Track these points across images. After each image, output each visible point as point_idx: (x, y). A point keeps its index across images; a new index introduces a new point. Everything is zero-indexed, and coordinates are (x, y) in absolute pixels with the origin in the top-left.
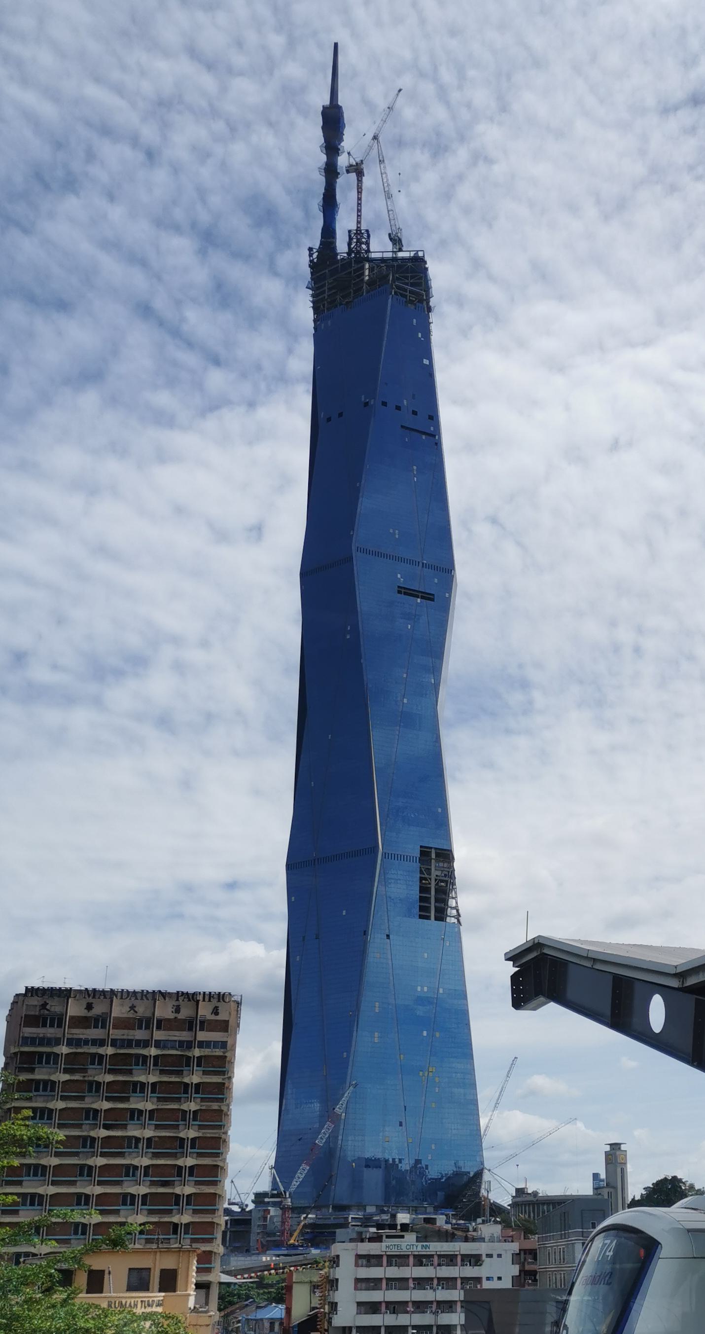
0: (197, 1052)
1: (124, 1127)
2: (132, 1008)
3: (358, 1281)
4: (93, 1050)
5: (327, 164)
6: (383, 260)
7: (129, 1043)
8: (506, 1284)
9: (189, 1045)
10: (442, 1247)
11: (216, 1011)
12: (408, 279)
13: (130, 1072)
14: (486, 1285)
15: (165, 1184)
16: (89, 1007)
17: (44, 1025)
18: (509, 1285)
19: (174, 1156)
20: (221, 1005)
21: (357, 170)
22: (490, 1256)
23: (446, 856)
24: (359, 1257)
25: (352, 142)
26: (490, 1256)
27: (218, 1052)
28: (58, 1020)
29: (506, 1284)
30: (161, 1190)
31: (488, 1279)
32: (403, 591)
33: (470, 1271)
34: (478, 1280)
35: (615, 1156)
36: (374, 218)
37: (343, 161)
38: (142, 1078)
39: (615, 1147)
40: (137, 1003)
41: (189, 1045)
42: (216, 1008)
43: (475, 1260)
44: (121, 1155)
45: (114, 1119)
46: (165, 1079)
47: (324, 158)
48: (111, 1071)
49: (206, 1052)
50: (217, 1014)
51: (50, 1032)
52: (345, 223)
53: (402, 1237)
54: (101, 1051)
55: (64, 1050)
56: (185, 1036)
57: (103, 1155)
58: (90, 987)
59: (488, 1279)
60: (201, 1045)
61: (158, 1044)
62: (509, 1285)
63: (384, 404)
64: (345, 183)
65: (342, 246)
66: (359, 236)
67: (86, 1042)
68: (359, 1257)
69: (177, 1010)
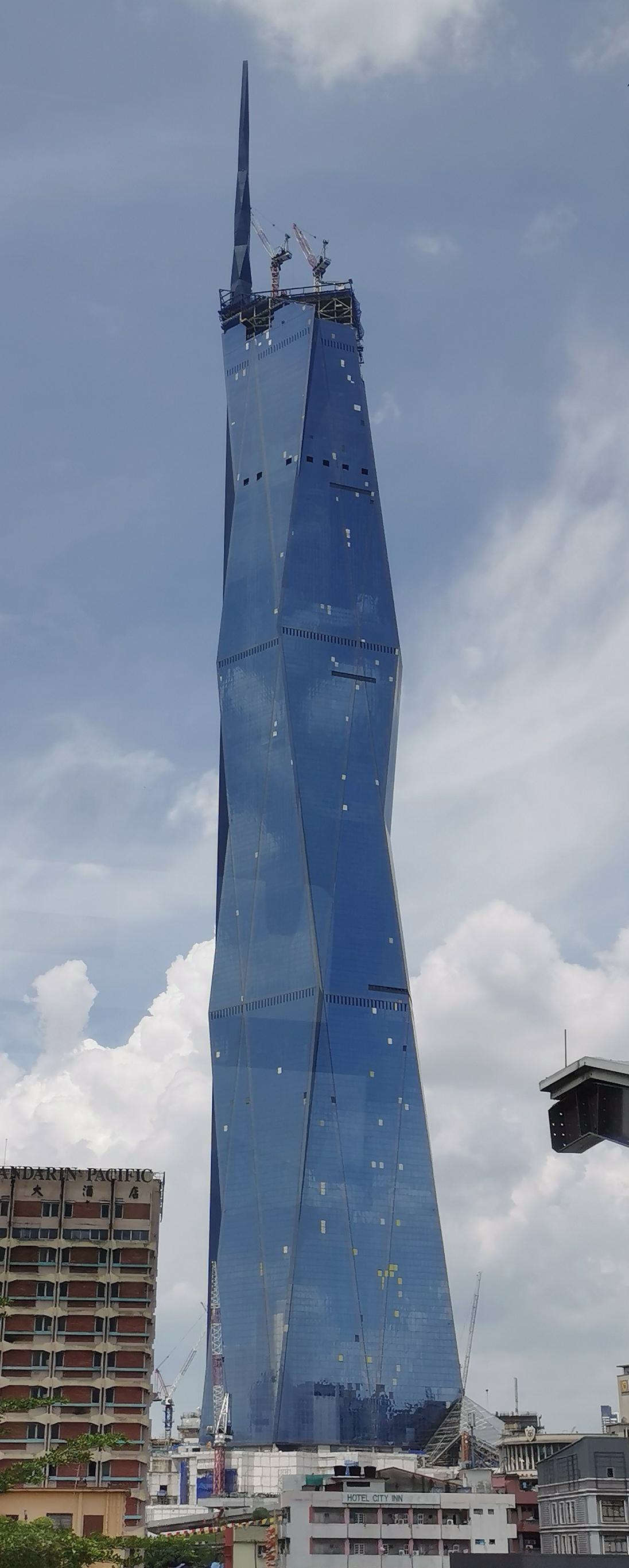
0: (113, 1244)
2: (37, 1189)
7: (34, 1234)
9: (104, 1235)
11: (134, 1193)
14: (476, 1549)
16: (89, 1192)
22: (479, 1511)
24: (315, 1510)
26: (479, 1511)
27: (139, 1244)
31: (478, 1541)
34: (466, 1543)
42: (135, 1189)
43: (461, 1516)
50: (136, 1196)
53: (368, 1485)
59: (478, 1541)
69: (89, 1192)
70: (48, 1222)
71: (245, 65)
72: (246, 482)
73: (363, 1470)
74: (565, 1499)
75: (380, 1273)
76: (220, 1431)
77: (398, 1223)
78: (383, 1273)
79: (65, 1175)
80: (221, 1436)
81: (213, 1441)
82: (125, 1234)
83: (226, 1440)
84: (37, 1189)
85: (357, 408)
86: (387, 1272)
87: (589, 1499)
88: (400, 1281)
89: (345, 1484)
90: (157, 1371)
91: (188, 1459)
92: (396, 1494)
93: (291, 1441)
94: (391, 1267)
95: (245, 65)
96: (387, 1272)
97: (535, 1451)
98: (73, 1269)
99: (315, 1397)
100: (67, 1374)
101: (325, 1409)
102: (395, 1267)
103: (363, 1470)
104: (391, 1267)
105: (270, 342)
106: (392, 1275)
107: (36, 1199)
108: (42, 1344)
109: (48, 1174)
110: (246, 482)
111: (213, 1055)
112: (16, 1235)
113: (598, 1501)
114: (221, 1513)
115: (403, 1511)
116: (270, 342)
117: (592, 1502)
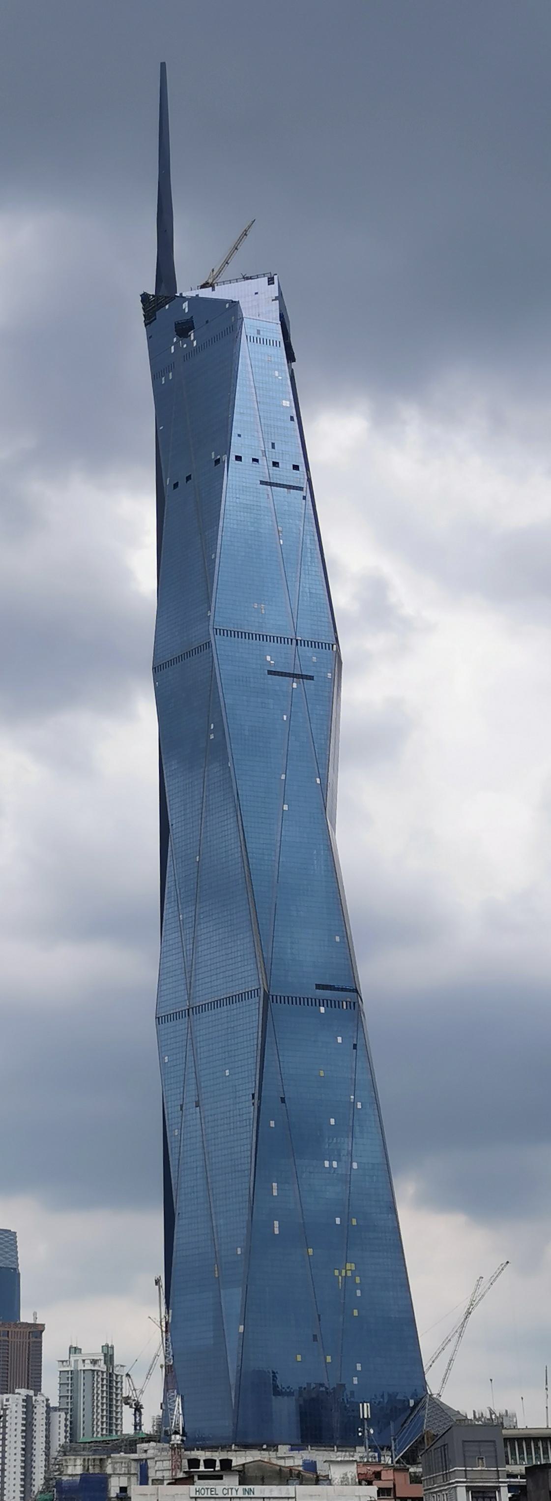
10: (271, 1491)
71: (163, 65)
72: (176, 485)
73: (218, 1463)
74: (441, 1491)
75: (337, 1272)
76: (176, 1433)
77: (354, 1222)
78: (340, 1273)
80: (178, 1437)
81: (169, 1441)
83: (182, 1440)
85: (227, 306)
86: (344, 1271)
87: (458, 1489)
88: (358, 1280)
89: (196, 1478)
90: (128, 1375)
91: (146, 1460)
92: (247, 1487)
93: (250, 1441)
94: (348, 1266)
95: (163, 65)
96: (344, 1271)
97: (537, 1448)
99: (273, 1397)
101: (285, 1410)
102: (353, 1267)
103: (218, 1463)
104: (348, 1266)
105: (195, 343)
106: (349, 1274)
110: (176, 485)
111: (161, 1058)
113: (467, 1491)
116: (195, 343)
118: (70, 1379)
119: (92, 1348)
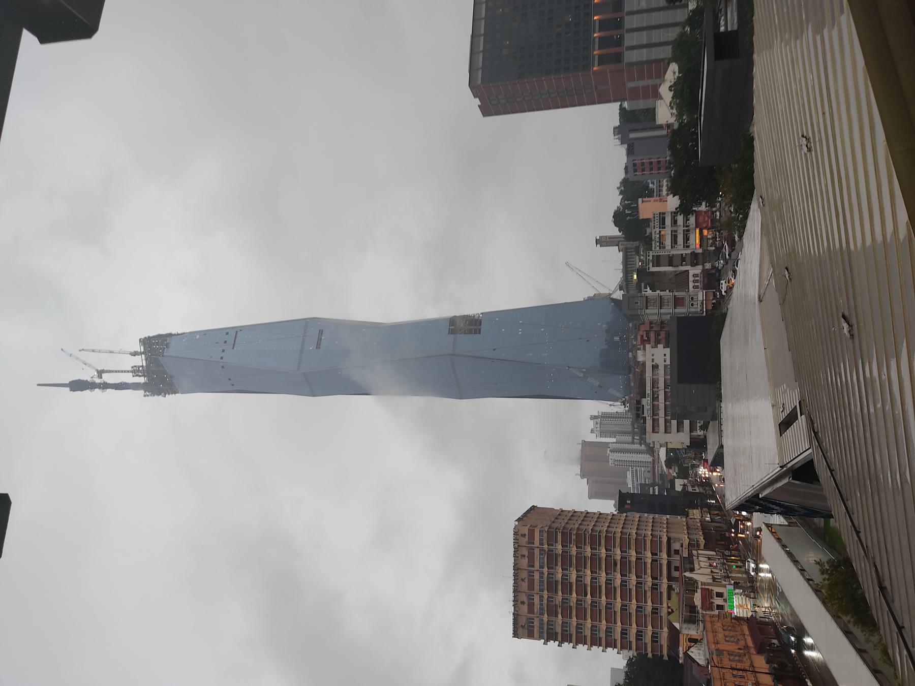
1: (585, 585)
2: (523, 580)
3: (666, 432)
4: (545, 602)
5: (100, 388)
6: (146, 359)
7: (541, 582)
8: (668, 351)
11: (524, 535)
12: (155, 346)
13: (556, 582)
14: (668, 362)
15: (615, 564)
16: (523, 603)
17: (533, 627)
18: (669, 349)
19: (600, 559)
20: (520, 533)
21: (100, 373)
22: (653, 360)
23: (453, 321)
24: (653, 431)
25: (87, 375)
26: (653, 360)
28: (530, 621)
29: (668, 351)
30: (619, 566)
32: (318, 346)
33: (661, 371)
34: (665, 366)
35: (602, 242)
36: (127, 362)
37: (98, 381)
38: (560, 576)
39: (597, 242)
40: (526, 539)
41: (542, 550)
43: (655, 367)
44: (600, 587)
45: (581, 590)
46: (560, 564)
47: (97, 390)
48: (556, 592)
49: (545, 541)
51: (536, 623)
52: (129, 378)
54: (546, 597)
55: (545, 618)
56: (537, 552)
57: (600, 597)
58: (512, 603)
60: (541, 544)
61: (542, 567)
62: (669, 349)
63: (222, 358)
64: (108, 378)
65: (142, 380)
66: (135, 371)
67: (541, 605)
68: (653, 431)
69: (523, 556)
70: (537, 576)
79: (516, 568)
82: (541, 540)
84: (523, 580)
98: (556, 565)
100: (600, 569)
107: (526, 581)
108: (588, 580)
109: (516, 575)
112: (542, 614)
114: (705, 228)
115: (653, 393)
117: (647, 311)
118: (603, 434)
119: (591, 424)
